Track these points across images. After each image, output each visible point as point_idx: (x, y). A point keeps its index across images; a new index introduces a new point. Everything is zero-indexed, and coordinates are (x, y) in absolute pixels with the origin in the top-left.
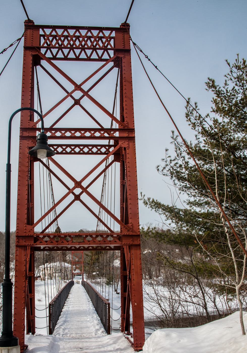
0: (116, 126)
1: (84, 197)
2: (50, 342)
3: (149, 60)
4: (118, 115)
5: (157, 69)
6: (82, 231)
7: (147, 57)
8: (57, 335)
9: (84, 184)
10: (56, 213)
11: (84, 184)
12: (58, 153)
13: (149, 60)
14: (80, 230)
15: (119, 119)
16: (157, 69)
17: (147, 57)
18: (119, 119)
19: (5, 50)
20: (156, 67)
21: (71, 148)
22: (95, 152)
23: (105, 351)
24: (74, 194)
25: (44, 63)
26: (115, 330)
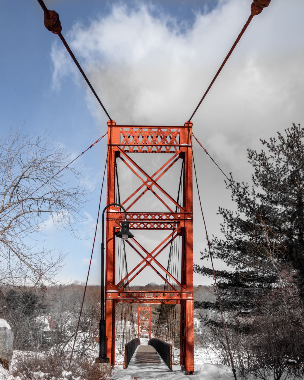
0: (179, 211)
1: (153, 263)
2: (128, 367)
3: (207, 153)
4: (181, 203)
5: (213, 161)
6: (150, 285)
7: (206, 151)
8: (157, 326)
9: (153, 255)
10: (127, 271)
11: (153, 255)
12: (134, 229)
13: (207, 153)
14: (147, 285)
15: (182, 206)
16: (213, 161)
17: (206, 151)
18: (182, 206)
19: (92, 146)
20: (213, 160)
21: (144, 225)
22: (162, 227)
23: (168, 379)
24: (146, 261)
25: (122, 155)
26: (161, 221)
